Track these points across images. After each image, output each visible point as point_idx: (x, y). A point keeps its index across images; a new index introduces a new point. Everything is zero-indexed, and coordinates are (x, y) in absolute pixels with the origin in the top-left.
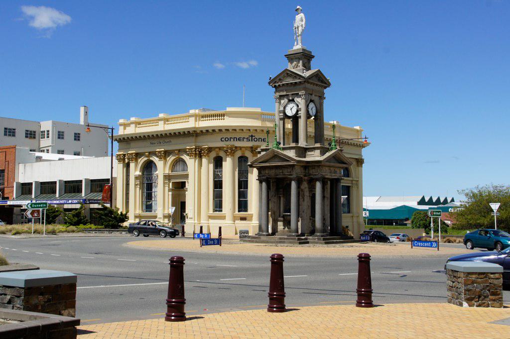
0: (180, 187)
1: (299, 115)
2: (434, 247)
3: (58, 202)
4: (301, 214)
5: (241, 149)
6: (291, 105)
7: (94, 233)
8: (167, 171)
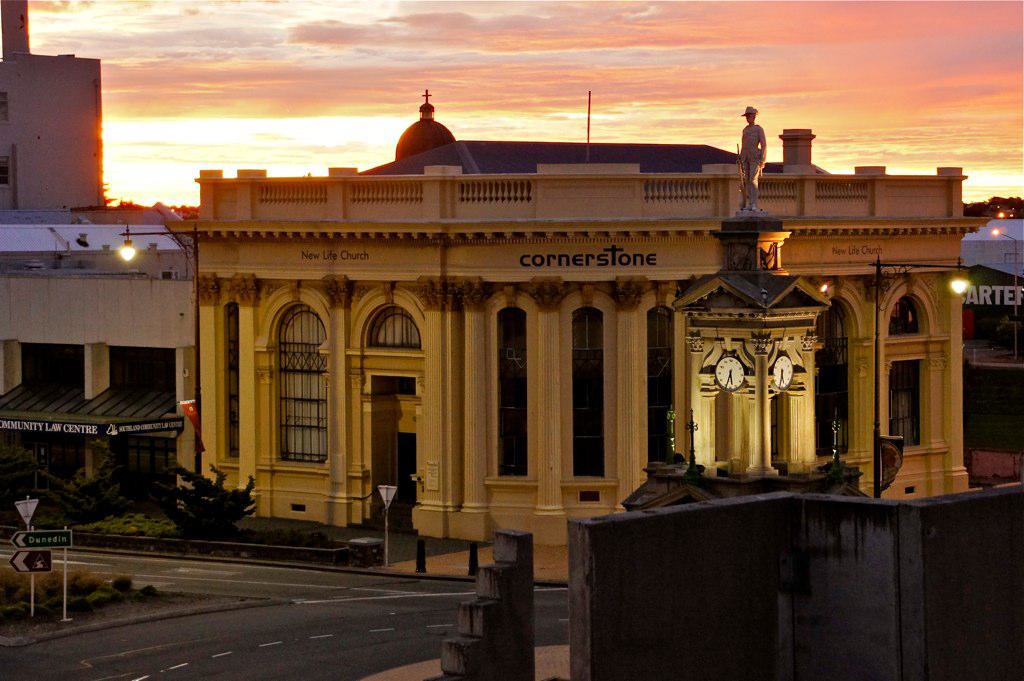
5: (581, 289)
7: (152, 548)
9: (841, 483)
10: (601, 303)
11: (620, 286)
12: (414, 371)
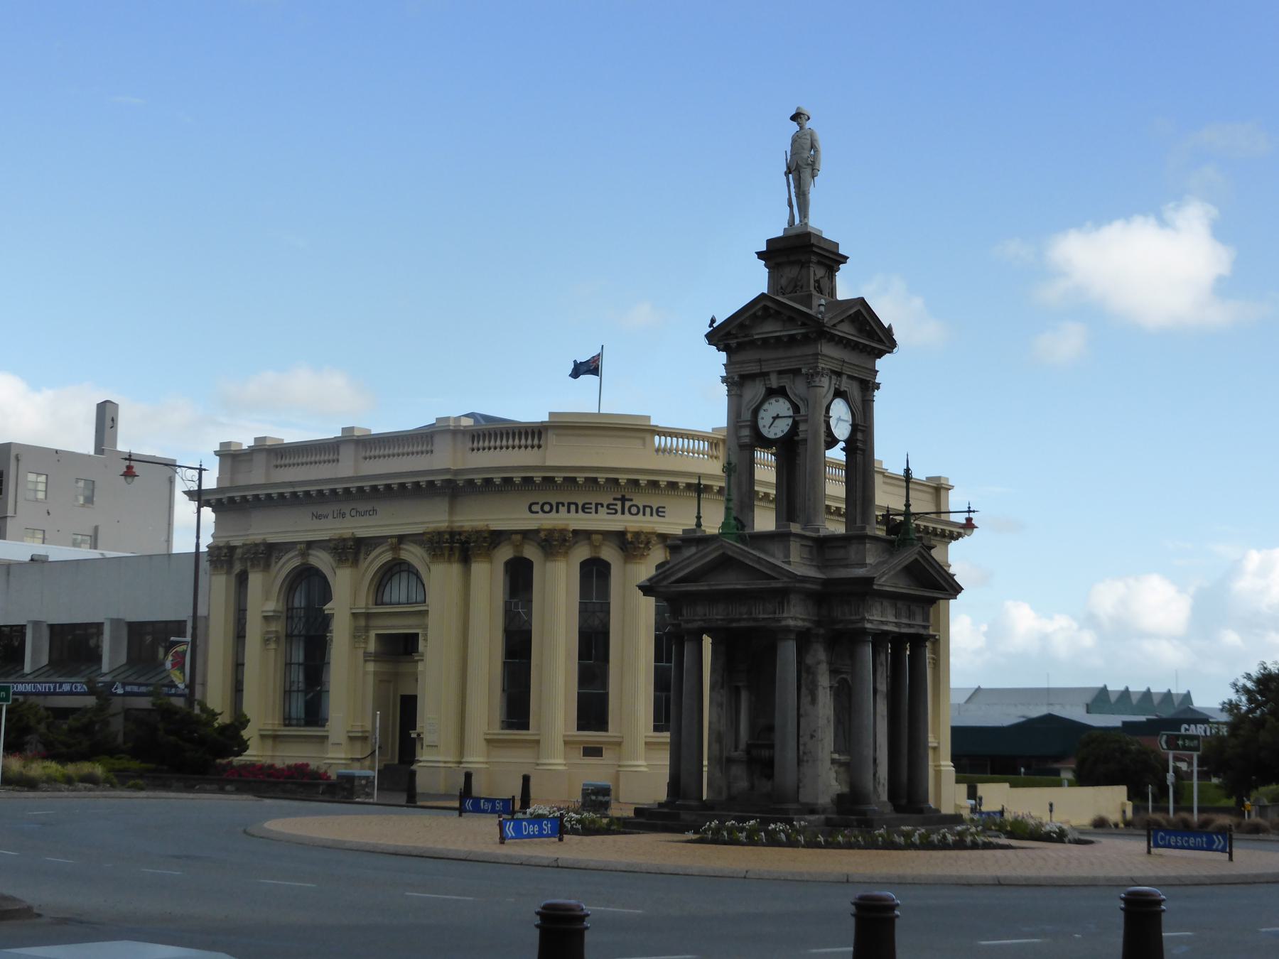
0: (401, 649)
1: (802, 436)
2: (1217, 850)
3: (29, 688)
4: (805, 745)
5: (589, 538)
6: (780, 407)
8: (361, 607)
9: (912, 545)
10: (609, 553)
11: (629, 536)
12: (417, 627)
